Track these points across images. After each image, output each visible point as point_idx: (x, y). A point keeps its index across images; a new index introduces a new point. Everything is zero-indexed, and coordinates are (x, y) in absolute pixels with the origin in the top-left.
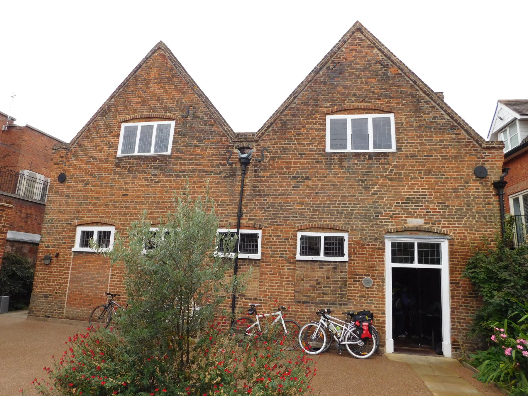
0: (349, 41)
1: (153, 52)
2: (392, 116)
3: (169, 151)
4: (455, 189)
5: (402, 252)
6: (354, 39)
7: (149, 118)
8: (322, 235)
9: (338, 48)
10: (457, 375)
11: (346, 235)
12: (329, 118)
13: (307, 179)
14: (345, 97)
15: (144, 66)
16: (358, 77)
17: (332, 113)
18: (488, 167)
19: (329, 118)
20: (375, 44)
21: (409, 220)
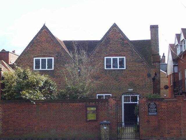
0: (112, 30)
1: (42, 29)
2: (125, 57)
3: (53, 69)
4: (142, 81)
5: (126, 99)
6: (113, 30)
7: (44, 56)
8: (104, 95)
9: (108, 32)
10: (125, 131)
11: (97, 96)
12: (105, 58)
13: (99, 78)
14: (110, 50)
15: (114, 54)
16: (115, 44)
17: (106, 56)
18: (151, 73)
19: (105, 58)
20: (120, 32)
21: (129, 89)
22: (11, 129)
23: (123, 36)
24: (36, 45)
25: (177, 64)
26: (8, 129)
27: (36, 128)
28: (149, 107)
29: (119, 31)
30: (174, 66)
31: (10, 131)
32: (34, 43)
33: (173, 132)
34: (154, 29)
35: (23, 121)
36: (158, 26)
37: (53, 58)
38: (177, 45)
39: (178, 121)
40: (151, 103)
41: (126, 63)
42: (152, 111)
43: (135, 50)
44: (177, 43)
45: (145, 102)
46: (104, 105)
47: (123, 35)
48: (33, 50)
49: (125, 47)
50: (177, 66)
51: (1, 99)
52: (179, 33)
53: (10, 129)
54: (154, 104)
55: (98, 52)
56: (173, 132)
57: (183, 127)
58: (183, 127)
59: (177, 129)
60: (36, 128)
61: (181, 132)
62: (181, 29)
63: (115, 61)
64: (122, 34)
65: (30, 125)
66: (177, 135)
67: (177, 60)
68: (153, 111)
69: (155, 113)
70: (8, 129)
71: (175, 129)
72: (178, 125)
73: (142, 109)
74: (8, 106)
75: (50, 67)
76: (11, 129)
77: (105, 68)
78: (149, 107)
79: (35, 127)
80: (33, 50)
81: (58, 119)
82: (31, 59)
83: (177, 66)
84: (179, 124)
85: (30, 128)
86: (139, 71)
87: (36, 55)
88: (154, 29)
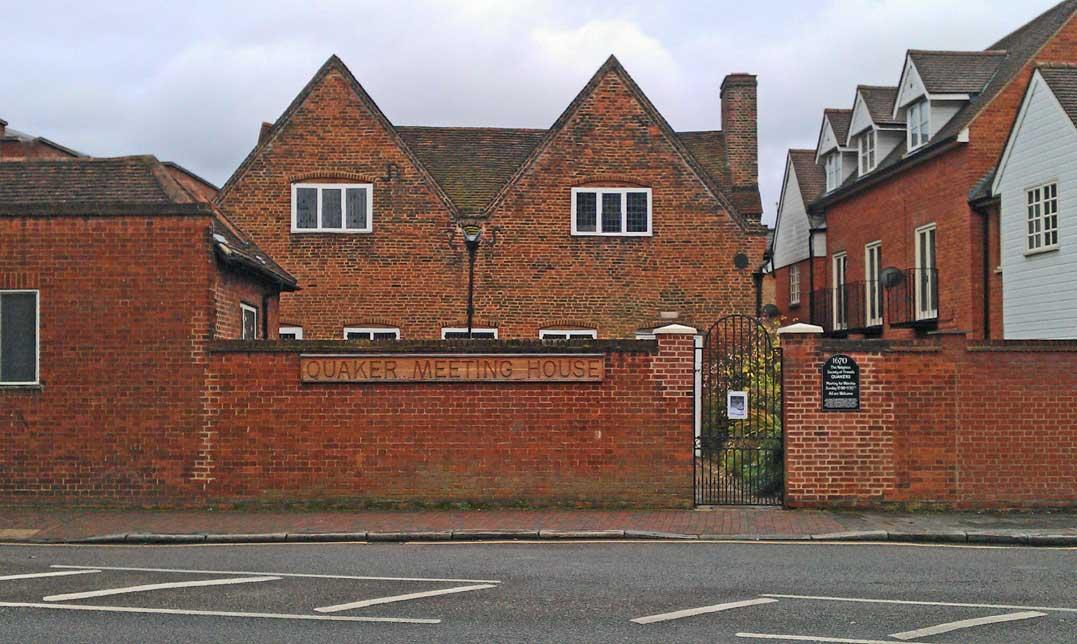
0: (601, 84)
3: (369, 229)
4: (713, 280)
6: (607, 82)
7: (334, 179)
18: (749, 254)
21: (662, 313)
22: (254, 464)
23: (645, 109)
24: (300, 131)
25: (823, 226)
26: (242, 464)
27: (360, 458)
28: (827, 377)
29: (627, 86)
30: (813, 232)
31: (250, 470)
32: (291, 124)
33: (920, 480)
34: (739, 90)
35: (304, 428)
36: (757, 78)
37: (369, 188)
38: (834, 151)
39: (942, 434)
40: (835, 360)
41: (654, 211)
42: (838, 391)
43: (688, 162)
44: (831, 142)
45: (809, 354)
46: (645, 366)
47: (642, 104)
48: (289, 153)
49: (652, 150)
50: (823, 231)
51: (1033, 195)
52: (846, 104)
53: (247, 464)
54: (846, 365)
55: (546, 170)
56: (920, 480)
57: (960, 462)
58: (960, 462)
59: (935, 468)
60: (360, 458)
61: (952, 480)
62: (856, 87)
63: (611, 201)
64: (638, 100)
65: (336, 446)
66: (937, 491)
67: (825, 208)
68: (843, 391)
69: (852, 402)
70: (242, 464)
71: (928, 468)
72: (944, 449)
73: (798, 383)
74: (239, 366)
75: (358, 219)
76: (254, 464)
77: (574, 232)
78: (827, 377)
79: (355, 453)
80: (289, 153)
81: (453, 423)
82: (279, 189)
83: (823, 231)
84: (944, 445)
85: (336, 457)
86: (704, 243)
87: (300, 174)
88: (739, 90)
